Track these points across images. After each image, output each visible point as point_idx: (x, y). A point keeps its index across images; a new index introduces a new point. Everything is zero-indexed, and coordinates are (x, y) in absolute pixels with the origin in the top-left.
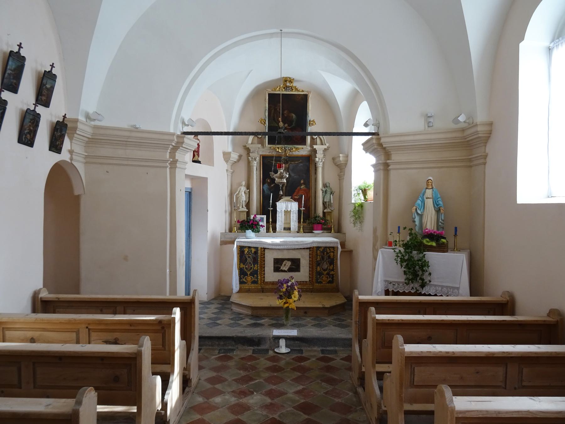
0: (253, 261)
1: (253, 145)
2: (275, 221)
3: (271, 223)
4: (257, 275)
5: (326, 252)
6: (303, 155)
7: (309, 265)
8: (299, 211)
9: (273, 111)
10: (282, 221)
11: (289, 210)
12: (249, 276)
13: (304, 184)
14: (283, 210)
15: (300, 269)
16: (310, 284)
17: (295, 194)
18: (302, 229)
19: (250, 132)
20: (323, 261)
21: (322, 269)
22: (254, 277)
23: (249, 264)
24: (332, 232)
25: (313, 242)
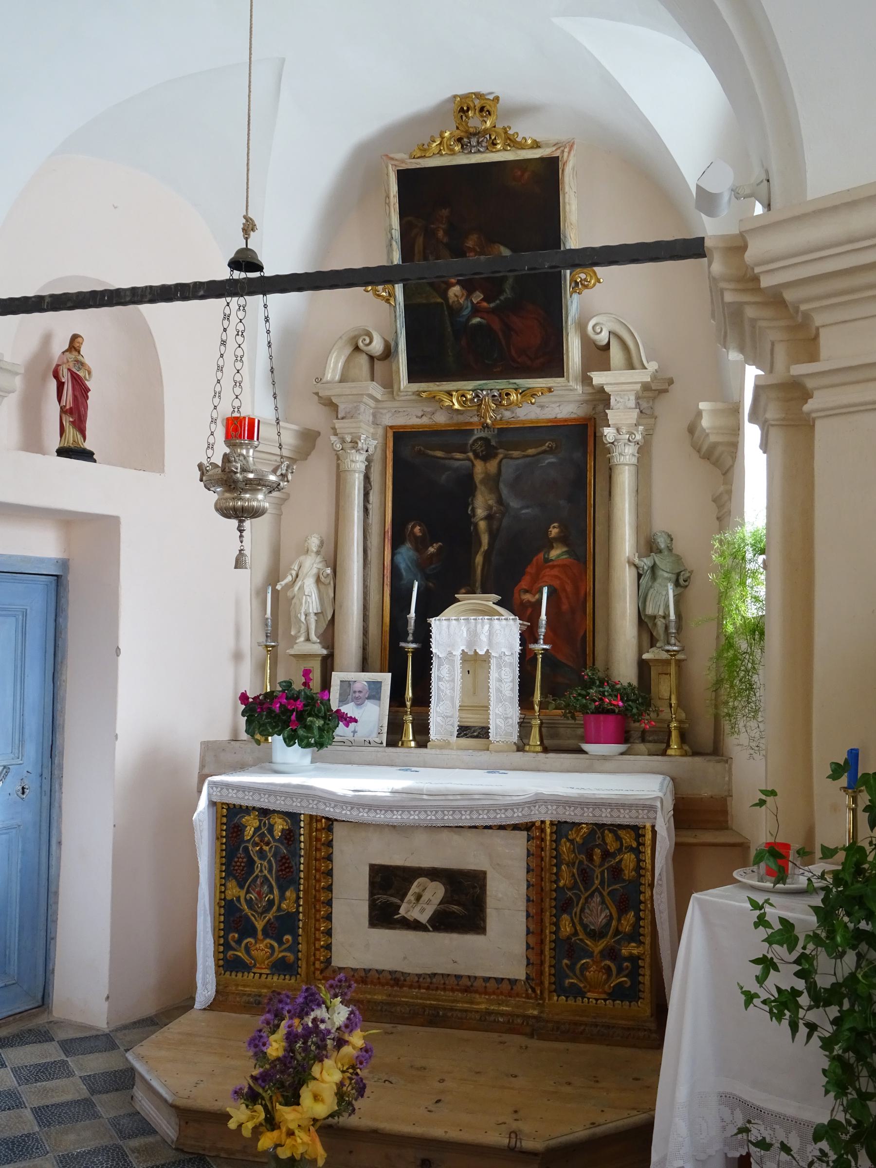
0: (277, 871)
1: (347, 388)
2: (423, 698)
3: (408, 704)
4: (296, 936)
5: (598, 846)
6: (560, 420)
7: (527, 907)
8: (526, 660)
9: (420, 241)
10: (452, 699)
11: (481, 652)
12: (260, 935)
13: (563, 539)
14: (458, 653)
15: (484, 921)
16: (528, 997)
17: (524, 584)
18: (535, 732)
19: (151, 287)
20: (586, 890)
21: (585, 927)
22: (280, 942)
23: (262, 884)
24: (669, 752)
25: (538, 801)
